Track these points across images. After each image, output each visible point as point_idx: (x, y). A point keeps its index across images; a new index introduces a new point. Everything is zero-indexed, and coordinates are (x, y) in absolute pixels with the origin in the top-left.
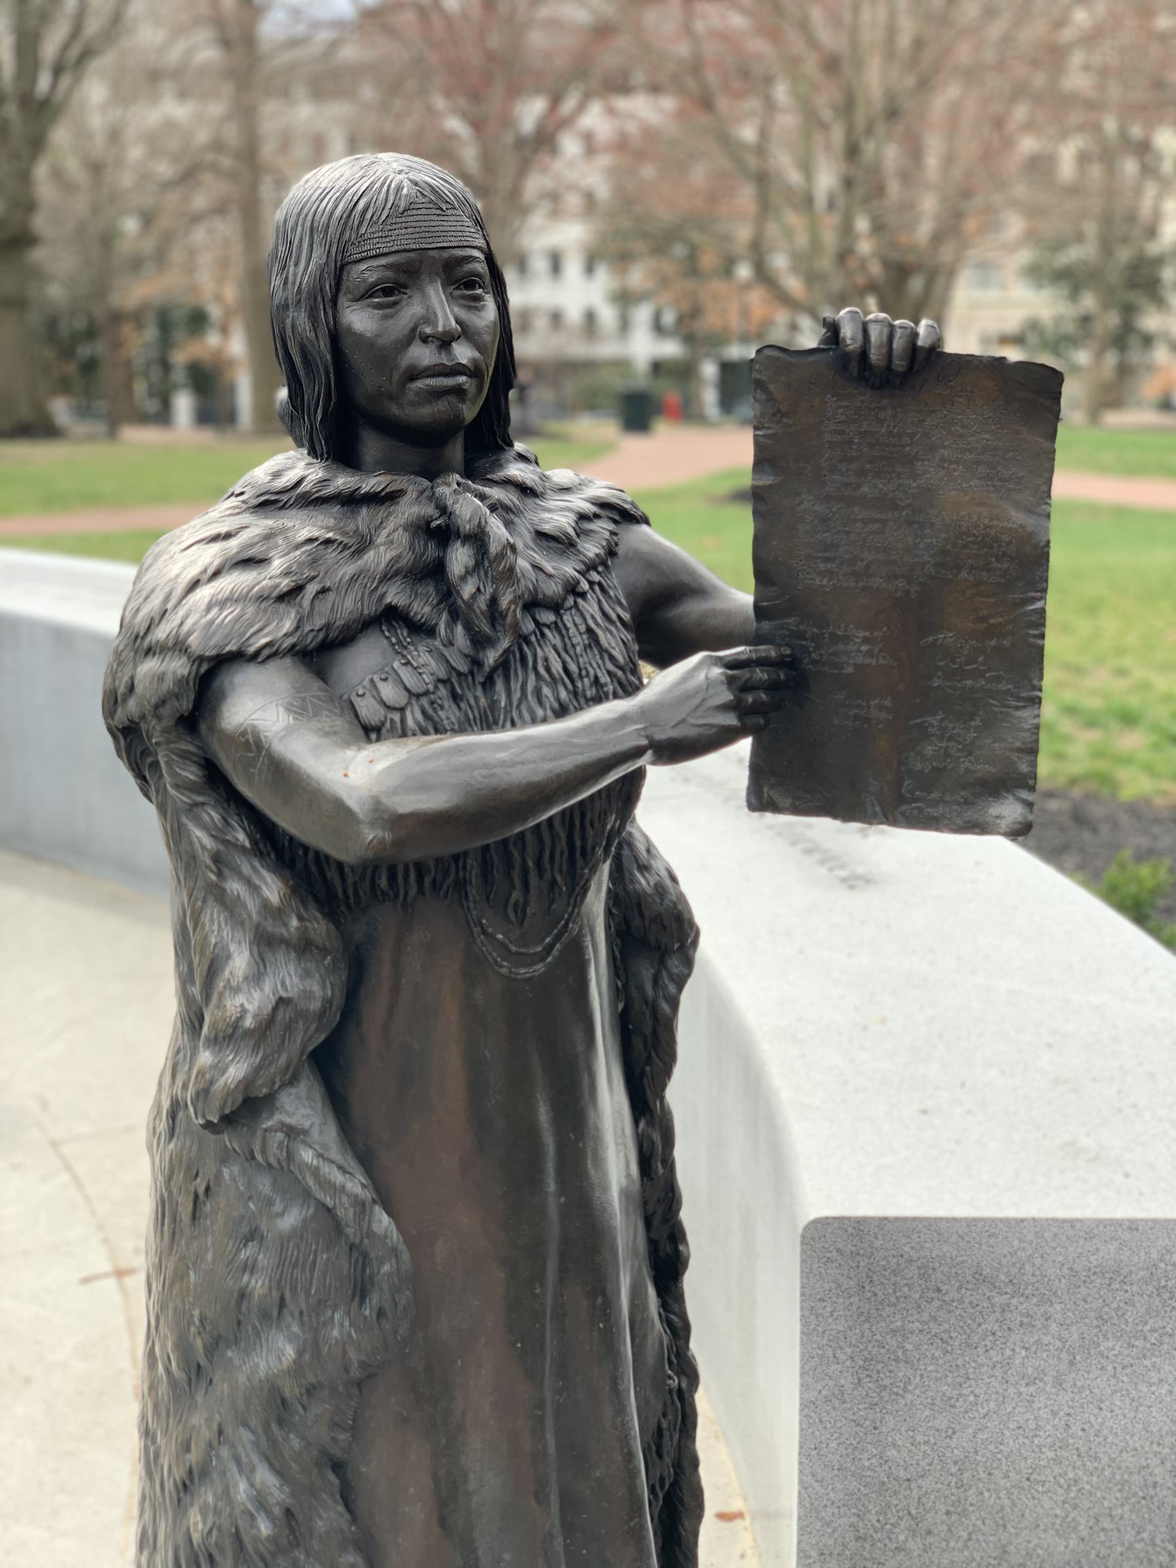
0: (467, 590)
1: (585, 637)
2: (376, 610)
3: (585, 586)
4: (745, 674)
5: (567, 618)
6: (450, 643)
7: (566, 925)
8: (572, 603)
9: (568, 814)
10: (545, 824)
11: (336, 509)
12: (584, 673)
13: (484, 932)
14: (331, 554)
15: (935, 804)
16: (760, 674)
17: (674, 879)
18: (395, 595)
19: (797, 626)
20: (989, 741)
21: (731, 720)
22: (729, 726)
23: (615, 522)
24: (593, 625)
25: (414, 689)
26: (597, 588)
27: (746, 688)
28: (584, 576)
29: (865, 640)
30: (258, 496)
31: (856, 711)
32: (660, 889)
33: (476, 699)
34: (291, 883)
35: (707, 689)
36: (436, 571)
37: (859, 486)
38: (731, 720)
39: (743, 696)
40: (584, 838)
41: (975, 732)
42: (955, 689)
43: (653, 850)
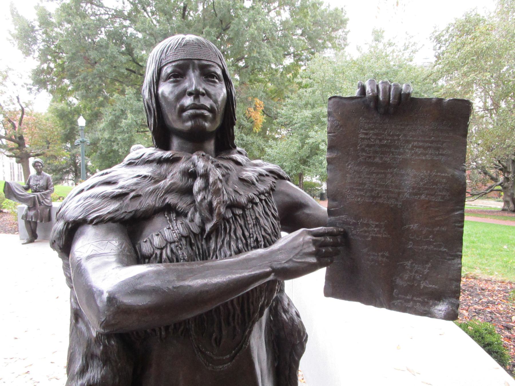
0: (199, 198)
1: (254, 221)
2: (161, 205)
3: (257, 200)
4: (322, 239)
5: (247, 212)
6: (192, 221)
7: (242, 346)
8: (251, 207)
9: (241, 299)
10: (229, 303)
11: (155, 164)
12: (251, 236)
13: (201, 351)
14: (146, 181)
15: (408, 301)
16: (329, 239)
17: (298, 315)
18: (171, 199)
19: (346, 219)
20: (435, 274)
21: (313, 260)
22: (313, 262)
23: (276, 179)
24: (258, 216)
25: (169, 240)
26: (263, 202)
27: (324, 245)
28: (258, 197)
29: (377, 226)
30: (128, 161)
31: (372, 257)
32: (292, 319)
33: (202, 245)
34: (231, 285)
35: (303, 245)
36: (188, 191)
37: (374, 158)
38: (313, 260)
39: (321, 249)
40: (249, 309)
41: (428, 270)
42: (420, 249)
43: (290, 303)
